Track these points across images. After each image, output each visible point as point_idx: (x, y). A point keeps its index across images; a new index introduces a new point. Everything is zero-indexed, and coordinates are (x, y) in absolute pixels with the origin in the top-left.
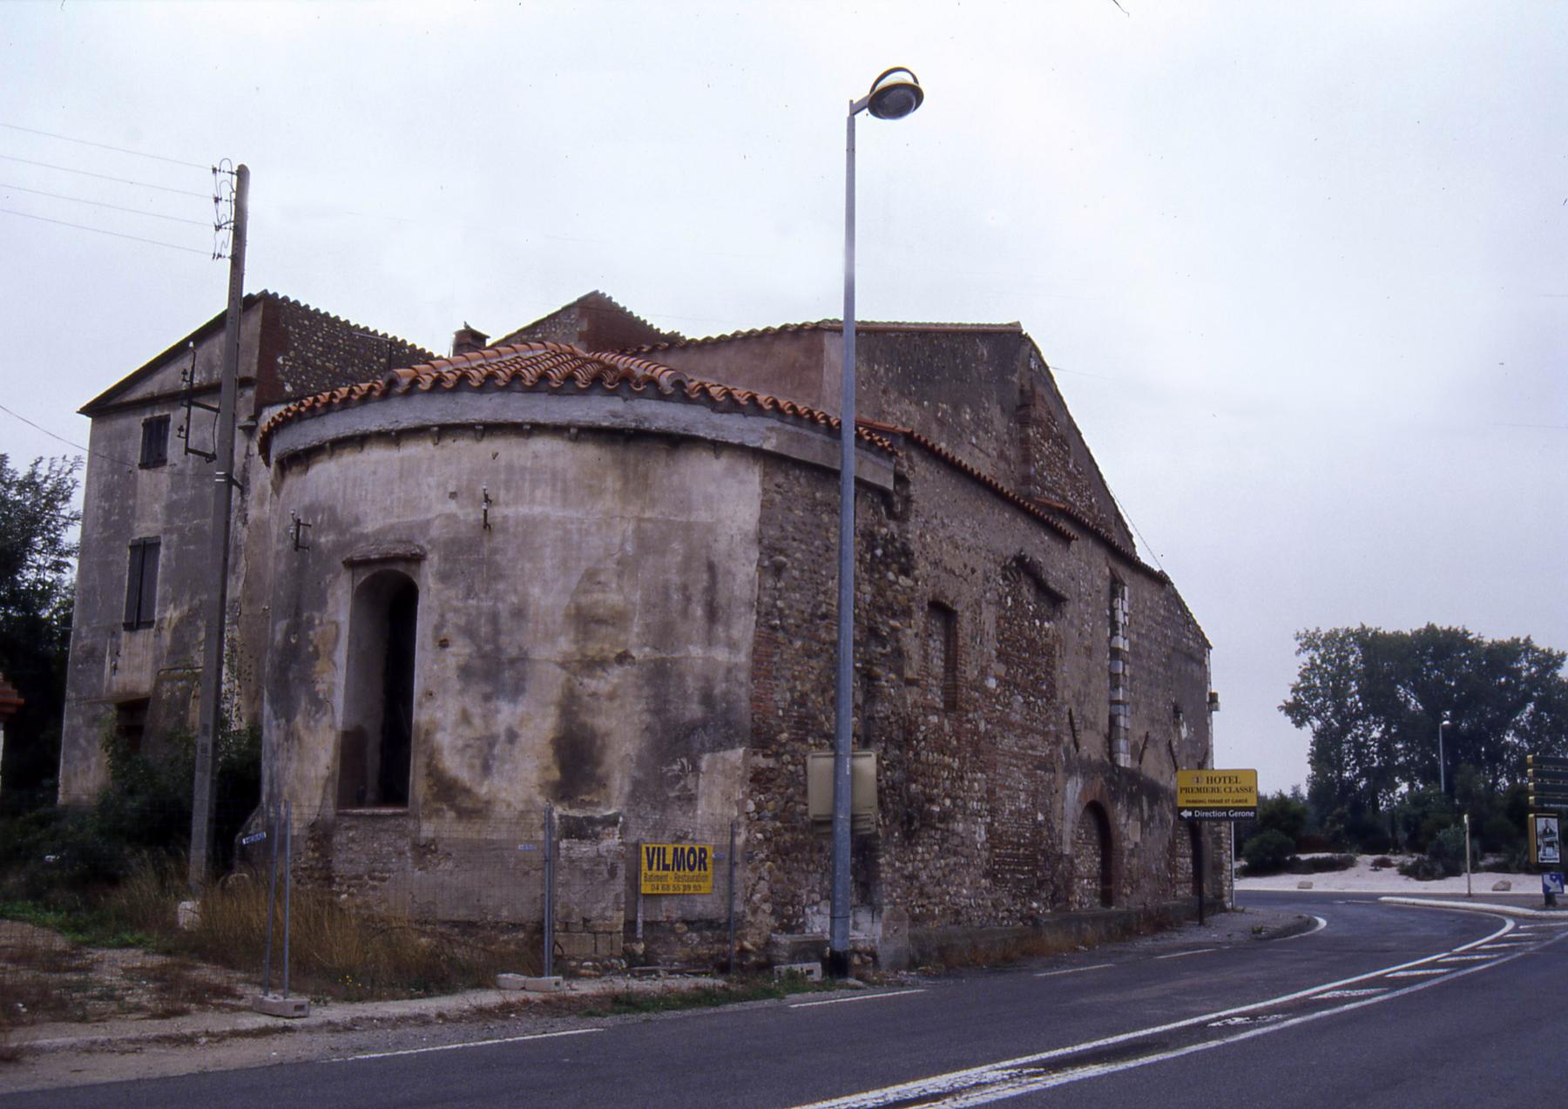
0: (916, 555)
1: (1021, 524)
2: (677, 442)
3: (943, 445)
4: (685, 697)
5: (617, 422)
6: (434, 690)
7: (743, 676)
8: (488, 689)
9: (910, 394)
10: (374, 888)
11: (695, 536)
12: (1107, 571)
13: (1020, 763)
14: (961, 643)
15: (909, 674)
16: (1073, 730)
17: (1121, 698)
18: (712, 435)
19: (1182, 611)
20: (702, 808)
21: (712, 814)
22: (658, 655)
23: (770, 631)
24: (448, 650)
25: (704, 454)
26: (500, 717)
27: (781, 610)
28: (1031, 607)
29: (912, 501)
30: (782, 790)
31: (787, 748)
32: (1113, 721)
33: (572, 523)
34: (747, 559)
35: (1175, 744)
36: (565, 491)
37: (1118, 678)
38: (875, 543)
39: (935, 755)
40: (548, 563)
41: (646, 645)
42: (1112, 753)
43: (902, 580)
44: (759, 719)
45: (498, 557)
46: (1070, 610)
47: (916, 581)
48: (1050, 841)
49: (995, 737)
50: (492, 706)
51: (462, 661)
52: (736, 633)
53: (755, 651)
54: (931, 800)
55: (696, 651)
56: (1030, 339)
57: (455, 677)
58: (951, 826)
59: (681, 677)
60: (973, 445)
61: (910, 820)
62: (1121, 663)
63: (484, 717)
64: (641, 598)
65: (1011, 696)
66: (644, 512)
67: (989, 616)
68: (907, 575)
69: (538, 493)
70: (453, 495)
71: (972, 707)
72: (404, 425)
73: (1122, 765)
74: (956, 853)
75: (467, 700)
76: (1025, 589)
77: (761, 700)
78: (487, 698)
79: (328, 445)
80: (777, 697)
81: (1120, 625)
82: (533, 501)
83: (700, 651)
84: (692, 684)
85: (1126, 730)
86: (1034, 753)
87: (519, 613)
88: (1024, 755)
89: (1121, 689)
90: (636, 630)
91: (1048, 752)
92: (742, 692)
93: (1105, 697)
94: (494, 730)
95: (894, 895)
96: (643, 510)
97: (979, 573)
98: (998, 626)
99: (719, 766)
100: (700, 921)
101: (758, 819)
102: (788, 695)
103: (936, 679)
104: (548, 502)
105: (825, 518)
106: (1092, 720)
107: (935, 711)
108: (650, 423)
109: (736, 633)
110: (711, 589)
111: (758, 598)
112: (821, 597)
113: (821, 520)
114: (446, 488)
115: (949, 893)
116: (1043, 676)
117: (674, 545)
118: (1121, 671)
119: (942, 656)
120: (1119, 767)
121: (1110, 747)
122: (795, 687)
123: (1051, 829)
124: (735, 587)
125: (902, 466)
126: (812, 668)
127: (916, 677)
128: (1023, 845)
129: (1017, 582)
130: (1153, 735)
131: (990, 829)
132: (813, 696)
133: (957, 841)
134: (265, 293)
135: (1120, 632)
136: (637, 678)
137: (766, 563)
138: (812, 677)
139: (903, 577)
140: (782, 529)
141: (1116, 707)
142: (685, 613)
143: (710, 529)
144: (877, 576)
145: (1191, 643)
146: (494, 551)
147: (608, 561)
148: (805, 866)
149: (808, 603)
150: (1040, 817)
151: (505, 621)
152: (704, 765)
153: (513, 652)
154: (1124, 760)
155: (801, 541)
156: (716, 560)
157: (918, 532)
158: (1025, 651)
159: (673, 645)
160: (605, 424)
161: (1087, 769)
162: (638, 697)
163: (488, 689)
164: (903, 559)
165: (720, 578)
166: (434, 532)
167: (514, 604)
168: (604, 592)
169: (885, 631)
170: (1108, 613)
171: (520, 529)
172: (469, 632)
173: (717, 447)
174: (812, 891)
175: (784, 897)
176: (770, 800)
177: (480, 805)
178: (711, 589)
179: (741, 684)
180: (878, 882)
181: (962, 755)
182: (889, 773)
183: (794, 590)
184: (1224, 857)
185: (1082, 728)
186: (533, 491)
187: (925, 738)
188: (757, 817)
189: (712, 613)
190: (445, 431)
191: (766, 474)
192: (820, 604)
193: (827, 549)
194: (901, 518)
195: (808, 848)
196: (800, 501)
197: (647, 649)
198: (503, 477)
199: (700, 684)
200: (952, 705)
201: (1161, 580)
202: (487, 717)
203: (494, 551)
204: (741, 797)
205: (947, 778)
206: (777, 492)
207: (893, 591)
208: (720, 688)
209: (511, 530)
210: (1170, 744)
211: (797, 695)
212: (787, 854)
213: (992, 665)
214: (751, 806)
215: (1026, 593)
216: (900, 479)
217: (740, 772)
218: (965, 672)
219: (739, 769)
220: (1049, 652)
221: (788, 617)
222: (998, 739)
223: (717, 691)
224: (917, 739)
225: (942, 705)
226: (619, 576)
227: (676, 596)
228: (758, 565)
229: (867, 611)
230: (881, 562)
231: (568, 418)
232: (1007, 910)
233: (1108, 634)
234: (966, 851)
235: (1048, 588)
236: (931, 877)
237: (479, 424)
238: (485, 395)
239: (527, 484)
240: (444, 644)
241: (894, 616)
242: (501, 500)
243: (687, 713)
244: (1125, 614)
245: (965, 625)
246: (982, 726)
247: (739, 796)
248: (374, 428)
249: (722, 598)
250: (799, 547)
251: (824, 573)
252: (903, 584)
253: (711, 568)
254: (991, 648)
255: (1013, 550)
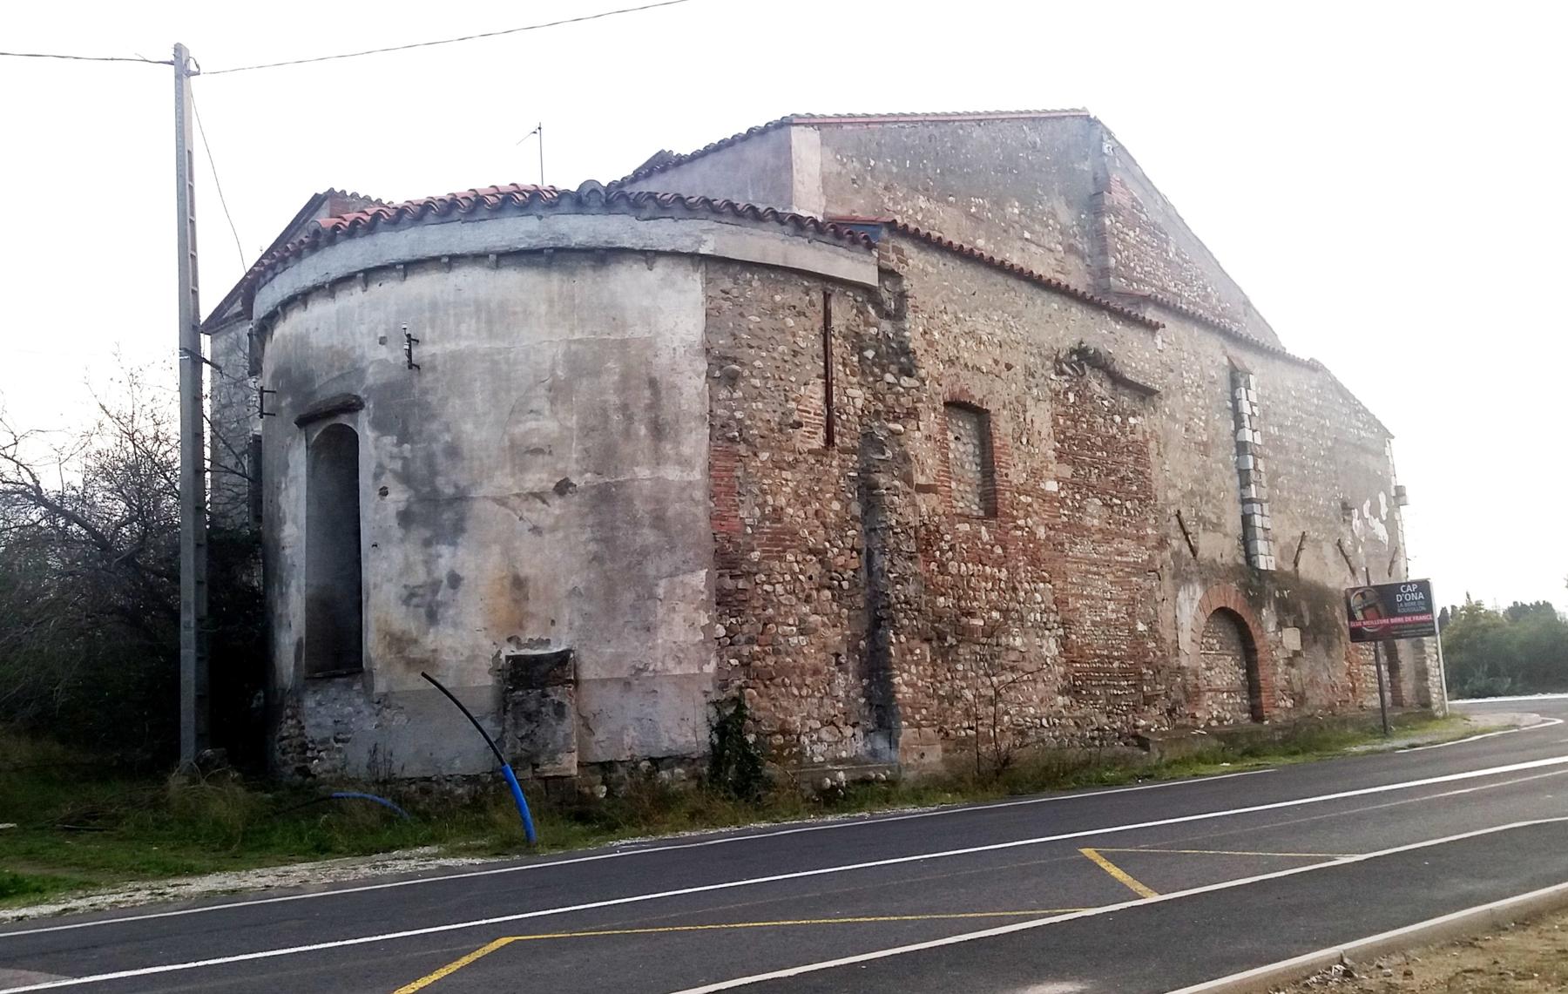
0: (919, 353)
1: (1077, 312)
2: (604, 256)
3: (981, 243)
4: (635, 523)
5: (534, 243)
6: (378, 541)
7: (699, 494)
8: (427, 533)
9: (927, 190)
10: (339, 750)
11: (633, 352)
12: (1225, 361)
13: (1103, 571)
14: (997, 443)
15: (921, 479)
16: (1186, 534)
17: (1254, 496)
18: (639, 245)
19: (1345, 398)
20: (662, 637)
21: (675, 642)
22: (601, 481)
23: (729, 444)
24: (387, 497)
25: (635, 267)
26: (442, 561)
27: (739, 421)
28: (1106, 403)
29: (907, 297)
30: (757, 612)
31: (762, 567)
32: (1246, 520)
33: (500, 353)
34: (694, 371)
35: (1348, 543)
36: (490, 322)
37: (1249, 474)
38: (864, 344)
39: (970, 565)
40: (478, 398)
41: (586, 471)
42: (1250, 556)
43: (905, 381)
44: (721, 538)
45: (429, 398)
46: (1167, 405)
47: (923, 381)
48: (1159, 653)
49: (1062, 544)
50: (432, 551)
51: (402, 506)
52: (686, 450)
53: (711, 467)
54: (970, 614)
55: (643, 472)
56: (1099, 122)
57: (396, 525)
58: (1003, 640)
59: (629, 500)
60: (1027, 239)
61: (941, 637)
62: (1250, 458)
63: (426, 562)
64: (578, 423)
65: (1083, 499)
66: (574, 334)
67: (1041, 417)
68: (910, 375)
69: (463, 328)
70: (383, 341)
71: (1021, 513)
72: (334, 275)
73: (1263, 566)
74: (1013, 669)
75: (408, 547)
76: (1094, 384)
77: (724, 518)
78: (427, 543)
79: (279, 309)
80: (743, 513)
81: (1246, 417)
82: (458, 336)
83: (648, 472)
84: (641, 508)
85: (1266, 530)
86: (1125, 559)
87: (453, 452)
88: (1110, 561)
89: (1253, 486)
90: (575, 456)
91: (1146, 557)
92: (700, 511)
93: (1234, 493)
94: (436, 575)
95: (918, 717)
96: (572, 331)
97: (1019, 368)
98: (1055, 423)
99: (679, 591)
100: (670, 757)
101: (731, 644)
102: (757, 511)
103: (970, 485)
104: (473, 334)
105: (790, 322)
106: (1215, 521)
107: (965, 518)
108: (569, 239)
109: (686, 450)
110: (654, 406)
111: (711, 411)
112: (793, 405)
113: (785, 324)
114: (376, 334)
115: (1008, 714)
116: (1131, 475)
117: (609, 364)
118: (1251, 466)
119: (978, 460)
120: (1259, 570)
121: (1247, 550)
122: (766, 502)
123: (1159, 640)
124: (683, 401)
125: (887, 259)
126: (787, 480)
127: (933, 483)
128: (1117, 659)
129: (1082, 376)
130: (1312, 534)
131: (1064, 642)
132: (790, 511)
133: (1013, 656)
134: (332, 191)
135: (1247, 423)
136: (580, 506)
137: (717, 374)
138: (788, 490)
139: (906, 378)
140: (735, 337)
141: (1248, 506)
142: (627, 434)
143: (649, 344)
144: (871, 379)
145: (1363, 433)
146: (425, 392)
147: (538, 389)
148: (796, 692)
149: (775, 412)
150: (1141, 627)
151: (442, 462)
152: (660, 591)
153: (449, 491)
154: (1265, 562)
155: (760, 348)
156: (657, 375)
157: (921, 329)
158: (1101, 450)
159: (616, 467)
160: (522, 246)
161: (1210, 573)
162: (582, 527)
163: (427, 533)
164: (902, 358)
165: (663, 393)
166: (370, 380)
167: (447, 442)
168: (537, 420)
169: (881, 435)
170: (1230, 405)
171: (448, 366)
172: (406, 478)
173: (649, 256)
174: (809, 717)
175: (770, 726)
176: (743, 623)
177: (428, 655)
178: (654, 406)
179: (697, 503)
180: (894, 703)
181: (1010, 564)
182: (898, 587)
183: (754, 401)
184: (1428, 662)
185: (1200, 531)
186: (458, 324)
187: (952, 548)
188: (729, 641)
189: (658, 431)
190: (370, 275)
191: (709, 281)
192: (791, 412)
193: (795, 354)
194: (897, 316)
195: (798, 671)
196: (755, 305)
197: (588, 475)
198: (427, 315)
199: (650, 507)
200: (991, 508)
201: (1313, 367)
202: (429, 563)
203: (425, 392)
204: (708, 622)
205: (992, 590)
206: (725, 300)
207: (894, 394)
208: (673, 509)
209: (439, 368)
210: (1339, 544)
211: (768, 510)
212: (771, 679)
213: (1050, 467)
214: (721, 631)
215: (1098, 389)
216: (885, 273)
217: (704, 597)
218: (1007, 475)
219: (702, 593)
220: (1140, 452)
221: (749, 428)
222: (1067, 546)
223: (670, 513)
224: (940, 549)
225: (981, 513)
226: (552, 403)
227: (616, 417)
228: (707, 376)
229: (859, 417)
230: (874, 364)
231: (484, 245)
232: (1098, 729)
233: (1233, 428)
234: (1028, 667)
235: (1126, 379)
236: (978, 696)
237: (400, 264)
238: (401, 232)
239: (452, 320)
240: (384, 492)
241: (896, 419)
242: (427, 339)
243: (638, 539)
244: (1252, 404)
245: (1003, 426)
246: (1041, 533)
247: (704, 620)
248: (309, 284)
249: (667, 415)
250: (759, 355)
251: (793, 379)
252: (906, 385)
253: (653, 384)
254: (1048, 448)
255: (1070, 342)
